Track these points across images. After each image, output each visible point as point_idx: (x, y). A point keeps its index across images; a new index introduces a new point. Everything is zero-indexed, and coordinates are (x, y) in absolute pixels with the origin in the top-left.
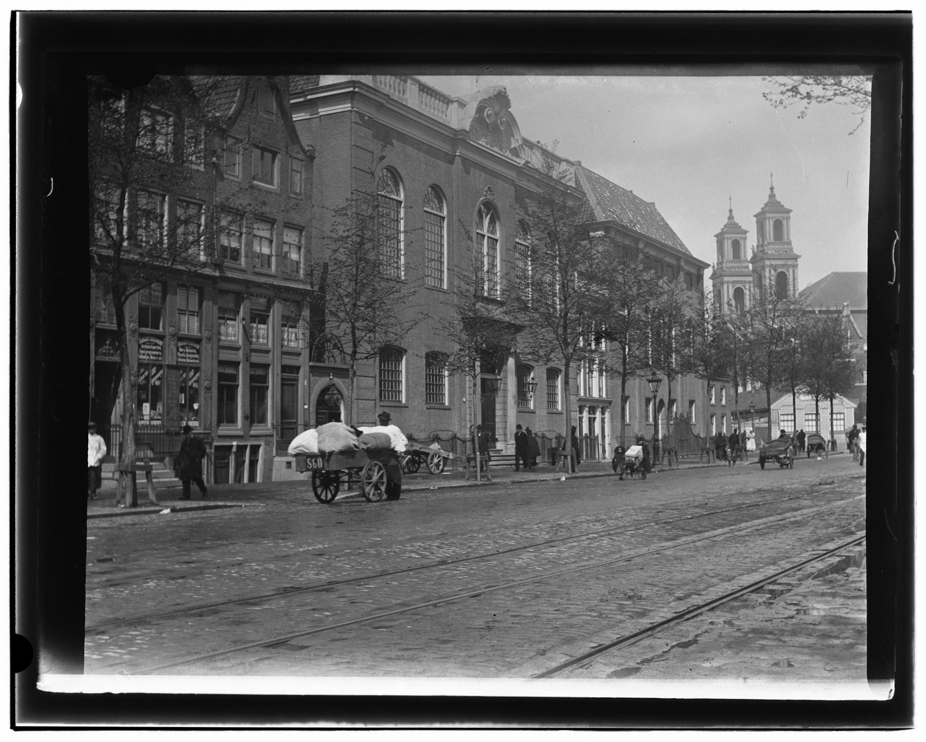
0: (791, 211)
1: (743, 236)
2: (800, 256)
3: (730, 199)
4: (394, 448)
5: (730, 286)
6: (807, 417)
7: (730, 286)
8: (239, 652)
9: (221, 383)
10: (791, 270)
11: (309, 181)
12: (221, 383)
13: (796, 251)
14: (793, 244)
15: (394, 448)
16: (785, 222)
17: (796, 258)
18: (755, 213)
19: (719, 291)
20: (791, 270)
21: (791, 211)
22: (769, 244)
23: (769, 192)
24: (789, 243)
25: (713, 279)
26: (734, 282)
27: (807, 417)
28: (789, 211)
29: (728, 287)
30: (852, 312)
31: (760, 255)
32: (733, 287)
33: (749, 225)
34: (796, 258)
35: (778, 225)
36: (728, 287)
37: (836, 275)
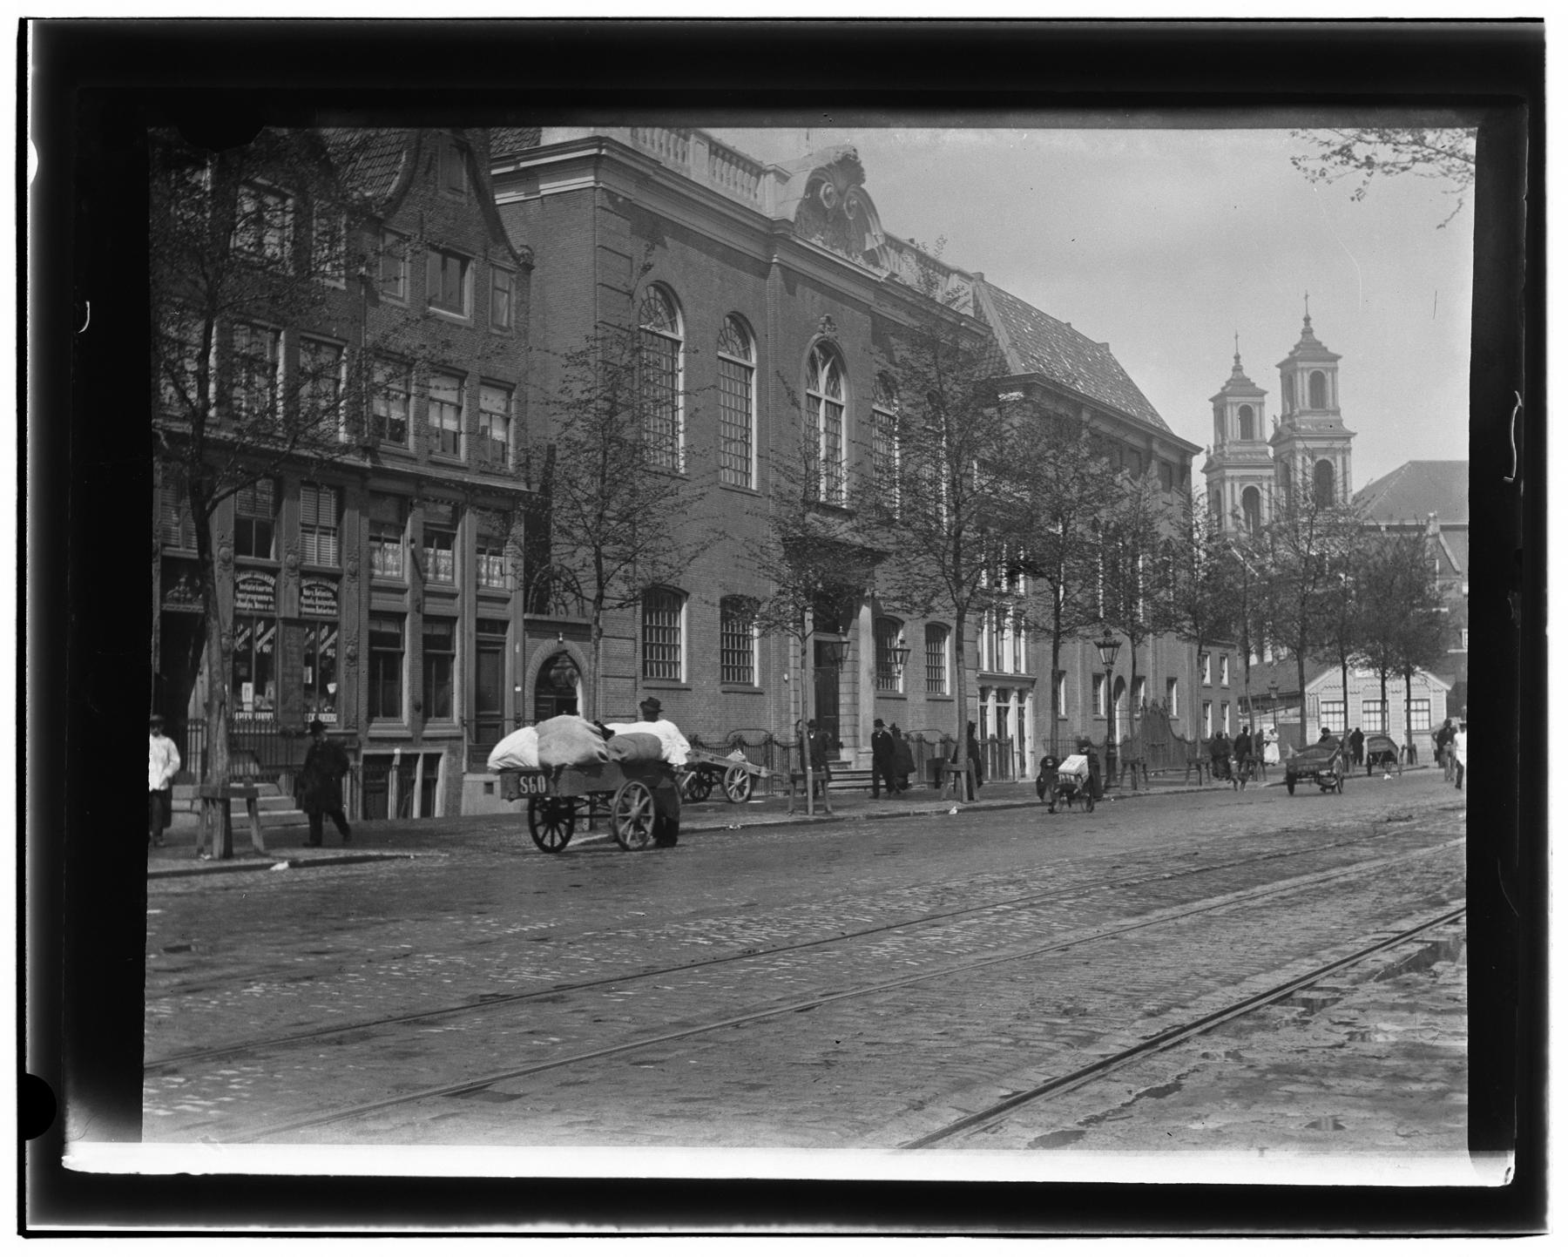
0: (1340, 357)
1: (1258, 399)
2: (1355, 434)
3: (1237, 337)
4: (667, 758)
5: (1237, 485)
6: (1366, 707)
7: (1237, 485)
8: (405, 1104)
9: (375, 648)
10: (1339, 458)
11: (523, 307)
12: (375, 648)
13: (1348, 425)
14: (1343, 414)
15: (667, 758)
16: (1328, 376)
17: (1348, 437)
18: (1279, 362)
19: (1218, 493)
20: (1339, 458)
21: (1340, 357)
22: (1302, 413)
23: (1302, 325)
24: (1337, 412)
25: (1207, 473)
26: (1242, 478)
27: (1366, 707)
28: (1336, 358)
29: (1233, 486)
30: (1443, 528)
31: (1287, 432)
32: (1241, 485)
33: (1269, 381)
34: (1348, 437)
35: (1318, 382)
36: (1233, 486)
37: (1416, 466)
